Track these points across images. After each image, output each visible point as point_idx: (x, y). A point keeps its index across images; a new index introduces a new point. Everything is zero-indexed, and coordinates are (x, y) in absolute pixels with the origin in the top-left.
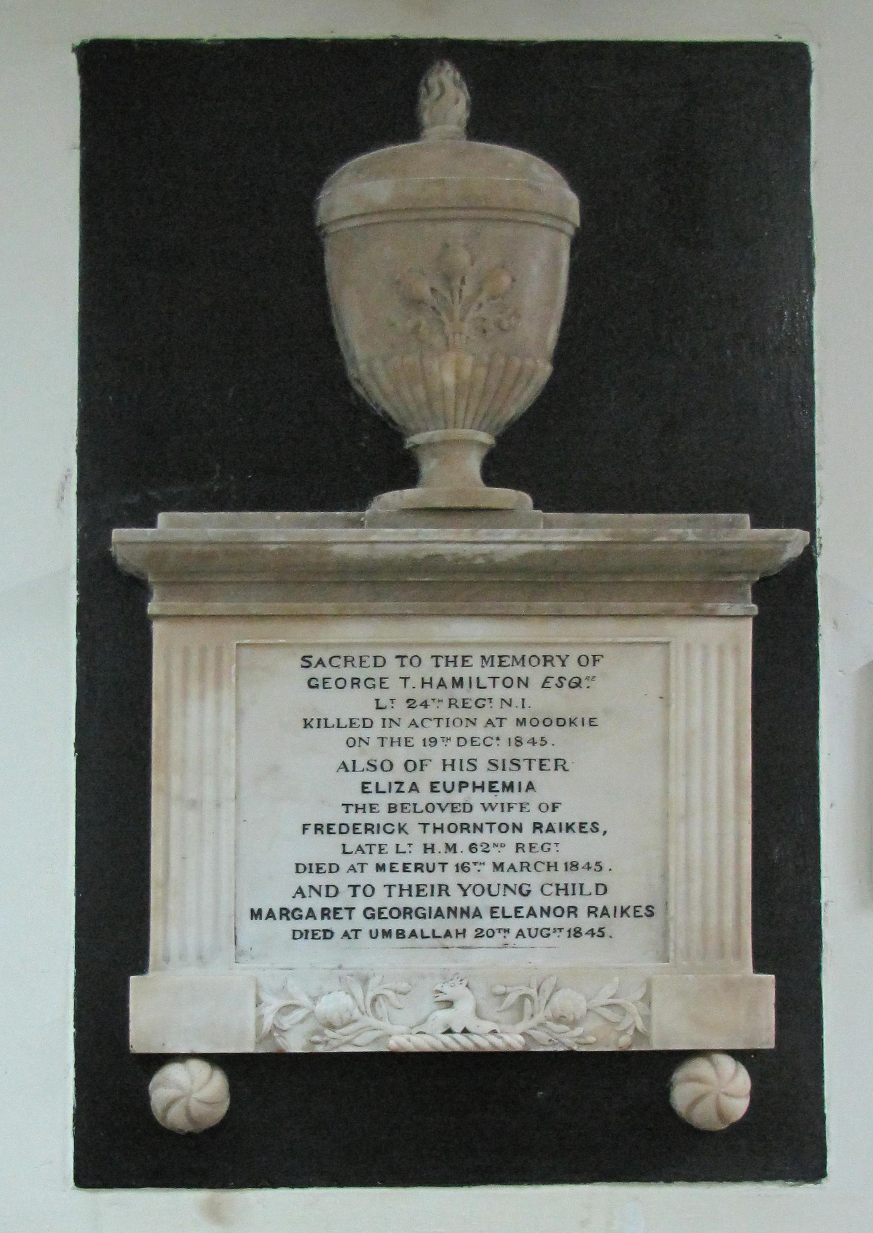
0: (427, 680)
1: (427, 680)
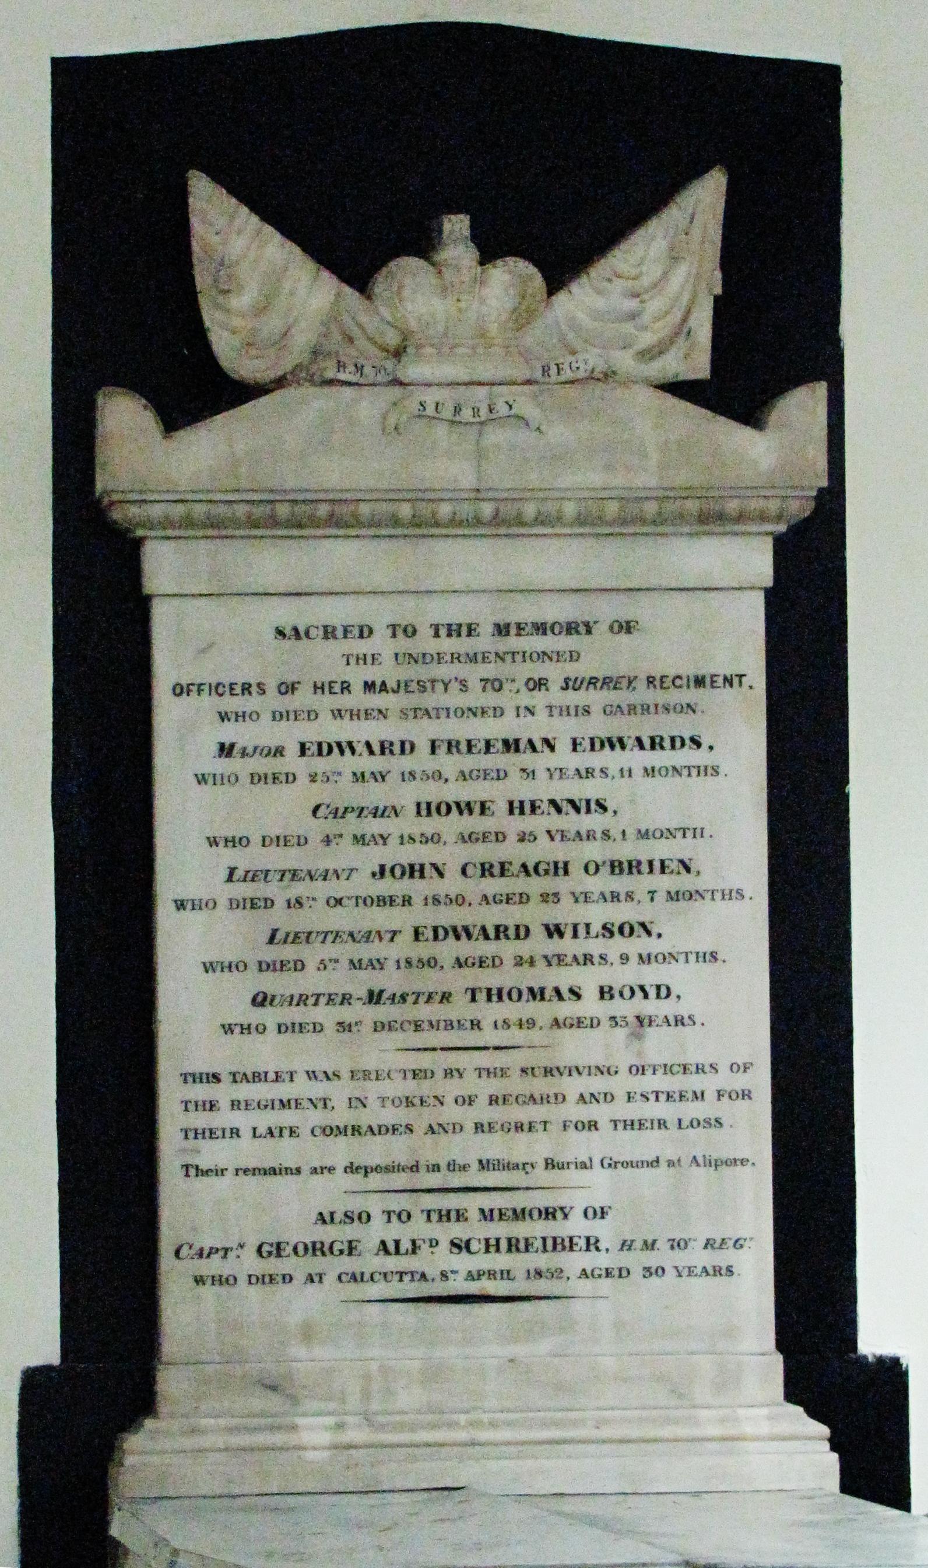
0: (319, 685)
1: (319, 685)
